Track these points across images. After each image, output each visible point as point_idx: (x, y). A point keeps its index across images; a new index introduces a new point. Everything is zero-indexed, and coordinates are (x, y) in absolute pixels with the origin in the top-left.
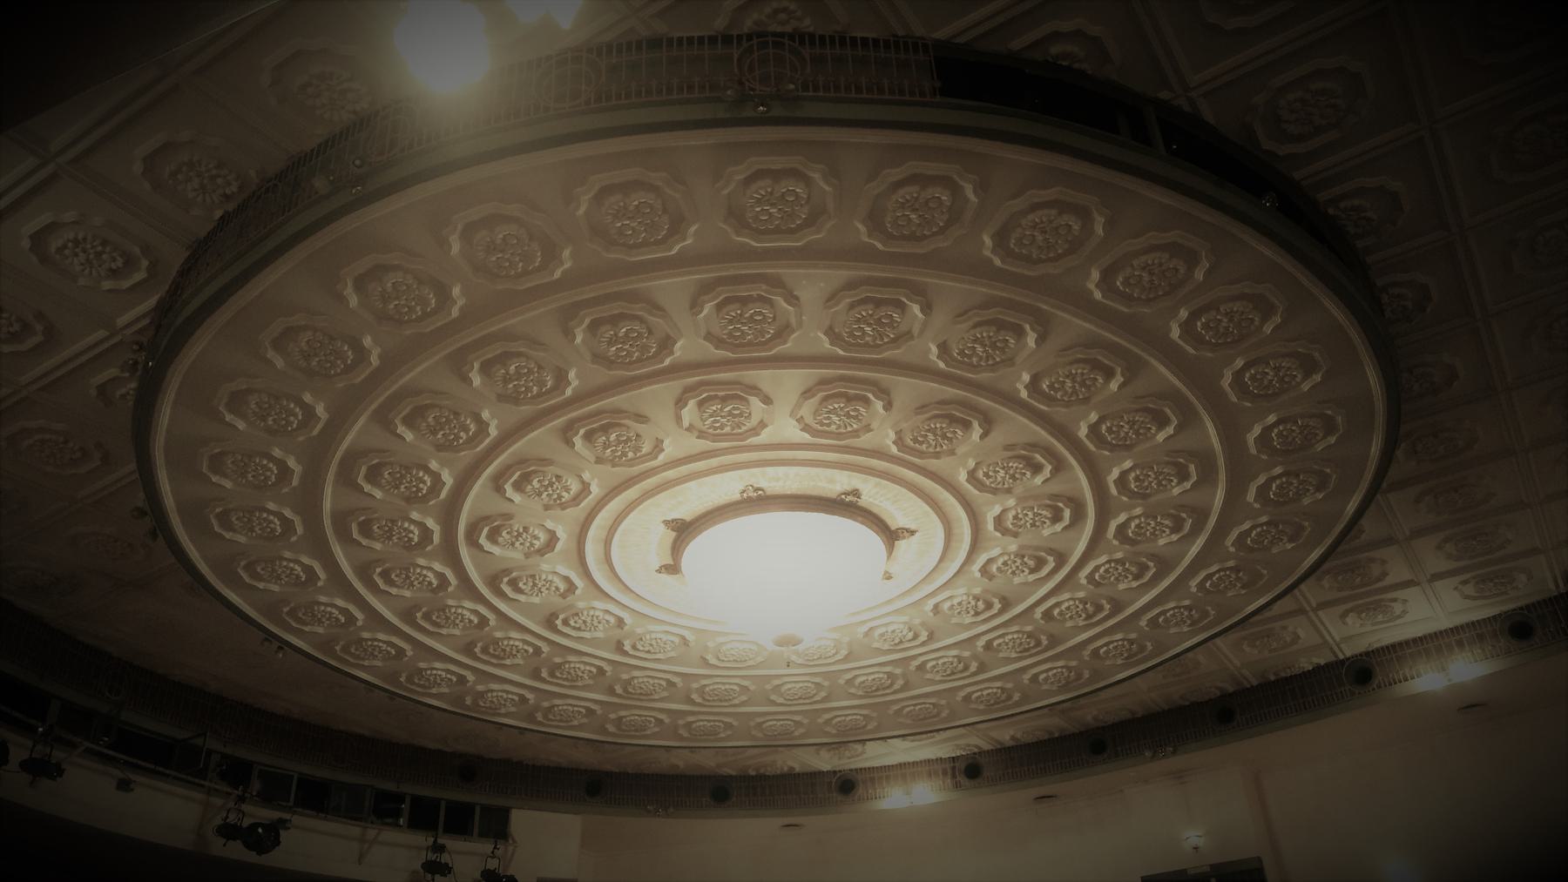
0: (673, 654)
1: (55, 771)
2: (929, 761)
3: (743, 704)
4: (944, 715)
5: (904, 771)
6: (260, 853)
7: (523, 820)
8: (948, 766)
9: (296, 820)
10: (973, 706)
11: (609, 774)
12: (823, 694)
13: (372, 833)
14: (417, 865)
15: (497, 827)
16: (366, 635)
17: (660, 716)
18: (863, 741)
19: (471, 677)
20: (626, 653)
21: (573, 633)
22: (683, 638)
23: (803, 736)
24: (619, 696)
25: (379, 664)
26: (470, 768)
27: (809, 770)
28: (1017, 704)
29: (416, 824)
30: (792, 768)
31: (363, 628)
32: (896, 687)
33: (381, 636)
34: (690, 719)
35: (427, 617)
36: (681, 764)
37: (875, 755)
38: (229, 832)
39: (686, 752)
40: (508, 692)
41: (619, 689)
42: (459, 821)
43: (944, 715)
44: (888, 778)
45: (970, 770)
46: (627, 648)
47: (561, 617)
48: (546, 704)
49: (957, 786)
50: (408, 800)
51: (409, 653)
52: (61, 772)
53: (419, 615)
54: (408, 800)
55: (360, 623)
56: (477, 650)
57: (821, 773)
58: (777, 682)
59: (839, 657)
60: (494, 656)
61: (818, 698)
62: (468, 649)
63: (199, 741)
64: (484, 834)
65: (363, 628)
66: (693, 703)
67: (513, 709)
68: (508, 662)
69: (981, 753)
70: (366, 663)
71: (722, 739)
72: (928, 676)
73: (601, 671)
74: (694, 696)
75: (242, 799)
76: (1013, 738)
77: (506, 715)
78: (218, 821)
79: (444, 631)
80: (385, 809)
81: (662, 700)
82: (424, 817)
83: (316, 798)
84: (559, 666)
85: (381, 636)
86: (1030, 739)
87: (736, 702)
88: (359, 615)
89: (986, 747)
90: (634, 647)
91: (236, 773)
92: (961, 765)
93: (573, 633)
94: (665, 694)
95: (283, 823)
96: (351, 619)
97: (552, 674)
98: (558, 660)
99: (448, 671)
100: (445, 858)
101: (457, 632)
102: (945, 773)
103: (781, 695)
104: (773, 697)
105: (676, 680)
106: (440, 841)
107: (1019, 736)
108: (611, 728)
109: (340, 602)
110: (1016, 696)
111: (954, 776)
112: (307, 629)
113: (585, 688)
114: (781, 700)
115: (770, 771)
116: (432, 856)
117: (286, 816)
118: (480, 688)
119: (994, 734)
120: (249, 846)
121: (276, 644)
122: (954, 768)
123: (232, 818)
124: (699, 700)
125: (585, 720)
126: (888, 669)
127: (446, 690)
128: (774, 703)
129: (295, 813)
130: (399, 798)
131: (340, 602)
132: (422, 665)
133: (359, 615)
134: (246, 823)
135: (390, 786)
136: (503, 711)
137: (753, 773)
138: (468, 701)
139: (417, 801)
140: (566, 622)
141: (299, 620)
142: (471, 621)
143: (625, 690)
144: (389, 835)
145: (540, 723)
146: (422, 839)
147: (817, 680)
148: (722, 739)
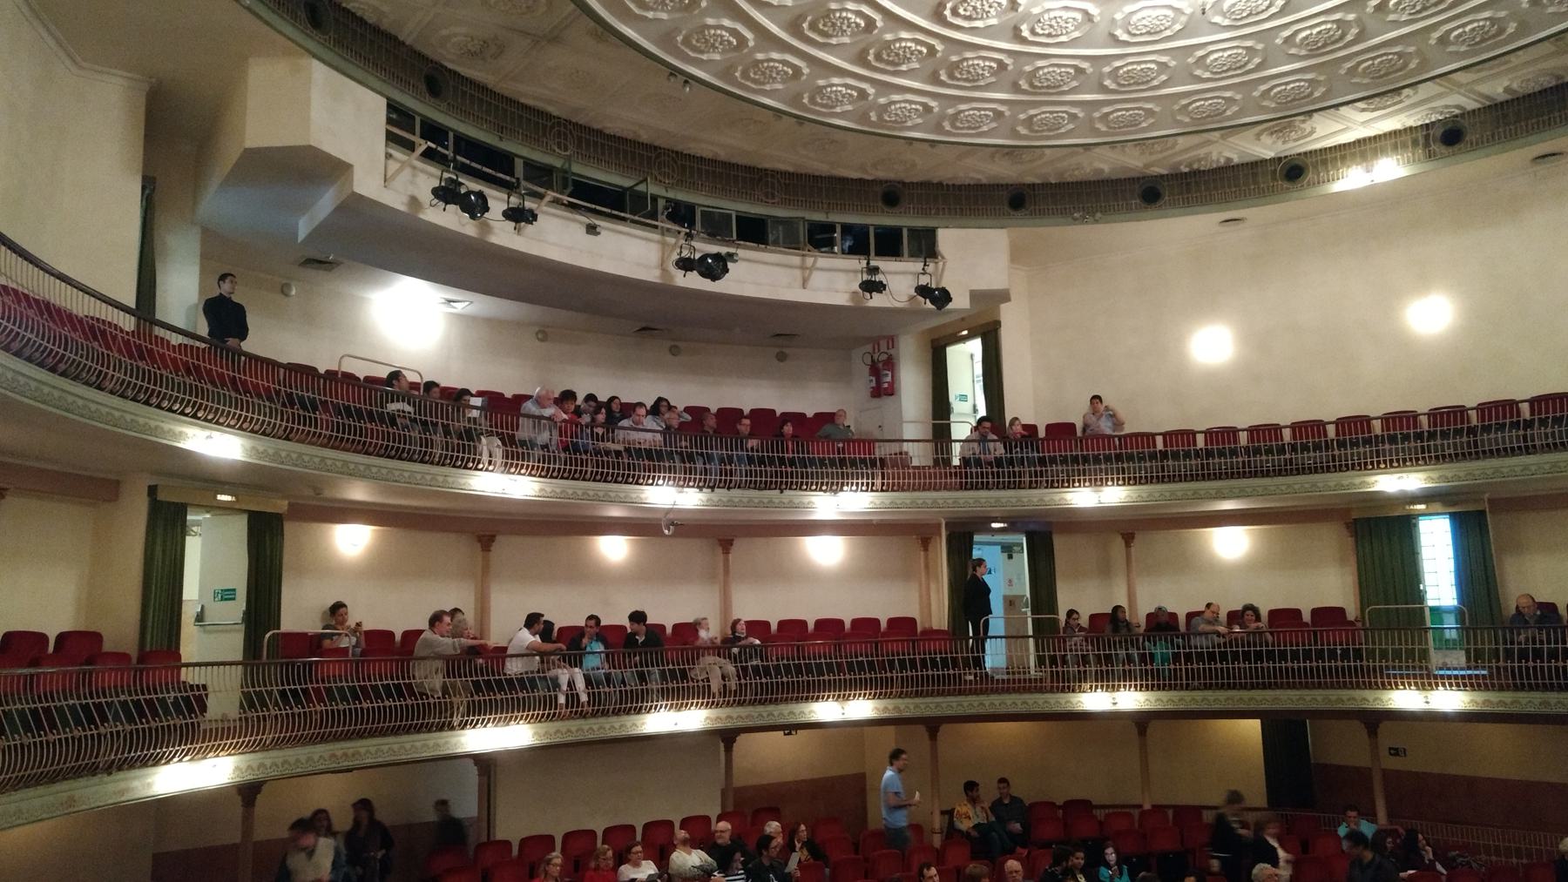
0: (1076, 34)
1: (530, 217)
2: (1395, 133)
3: (1164, 85)
4: (1412, 66)
5: (1365, 149)
6: (714, 278)
7: (948, 238)
8: (1420, 136)
9: (741, 253)
10: (1452, 48)
11: (1033, 186)
12: (1257, 60)
13: (809, 261)
14: (856, 287)
15: (926, 247)
16: (760, 56)
17: (1074, 110)
18: (1310, 113)
19: (871, 91)
20: (1024, 41)
21: (966, 24)
22: (1085, 12)
23: (1236, 115)
24: (1025, 92)
25: (780, 86)
26: (892, 195)
27: (1253, 159)
28: (1513, 37)
29: (853, 251)
30: (1229, 160)
31: (883, 31)
32: (1349, 38)
33: (775, 55)
34: (1106, 110)
35: (813, 27)
36: (1106, 168)
37: (1329, 131)
38: (685, 265)
39: (926, 145)
40: (911, 102)
41: (1024, 85)
42: (889, 244)
43: (1412, 66)
44: (1324, 162)
45: (1449, 136)
46: (1026, 33)
47: (949, 5)
48: (951, 111)
49: (1430, 156)
50: (839, 229)
51: (806, 71)
52: (535, 217)
53: (805, 25)
54: (839, 229)
55: (751, 44)
56: (871, 58)
57: (1264, 162)
58: (1200, 53)
59: (1273, 10)
60: (889, 63)
61: (1250, 66)
62: (861, 60)
63: (641, 188)
64: (914, 255)
65: (883, 31)
66: (1105, 90)
67: (919, 121)
68: (904, 68)
69: (1466, 114)
70: (768, 87)
71: (1144, 130)
72: (1392, 17)
73: (1002, 66)
74: (1107, 82)
75: (689, 236)
76: (1507, 90)
77: (914, 128)
78: (675, 257)
79: (834, 41)
80: (820, 238)
81: (1073, 91)
82: (858, 243)
83: (754, 232)
84: (957, 65)
85: (775, 55)
86: (1533, 87)
87: (1155, 83)
88: (749, 35)
89: (1471, 105)
90: (1033, 32)
91: (682, 215)
92: (1439, 132)
93: (966, 24)
94: (1075, 84)
95: (730, 256)
96: (742, 41)
97: (951, 76)
98: (954, 58)
99: (847, 86)
100: (879, 278)
101: (846, 40)
102: (1415, 143)
103: (1207, 68)
104: (1198, 72)
105: (1085, 65)
106: (873, 263)
107: (1515, 86)
108: (1022, 130)
109: (727, 23)
110: (1511, 28)
111: (1427, 145)
112: (705, 57)
113: (987, 88)
114: (1207, 75)
115: (1204, 166)
116: (866, 277)
117: (732, 250)
118: (882, 101)
119: (1485, 88)
120: (703, 275)
121: (681, 78)
122: (1427, 137)
123: (685, 254)
124: (1113, 86)
125: (994, 125)
126: (1337, 16)
127: (850, 108)
128: (1201, 80)
129: (738, 246)
130: (831, 228)
131: (727, 23)
132: (821, 82)
133: (749, 35)
134: (697, 256)
135: (819, 217)
136: (909, 124)
137: (1185, 170)
138: (873, 116)
139: (847, 229)
140: (955, 12)
141: (695, 49)
142: (858, 25)
143: (1031, 85)
144: (823, 261)
145: (949, 133)
146: (857, 263)
147: (1249, 43)
148: (1144, 130)
